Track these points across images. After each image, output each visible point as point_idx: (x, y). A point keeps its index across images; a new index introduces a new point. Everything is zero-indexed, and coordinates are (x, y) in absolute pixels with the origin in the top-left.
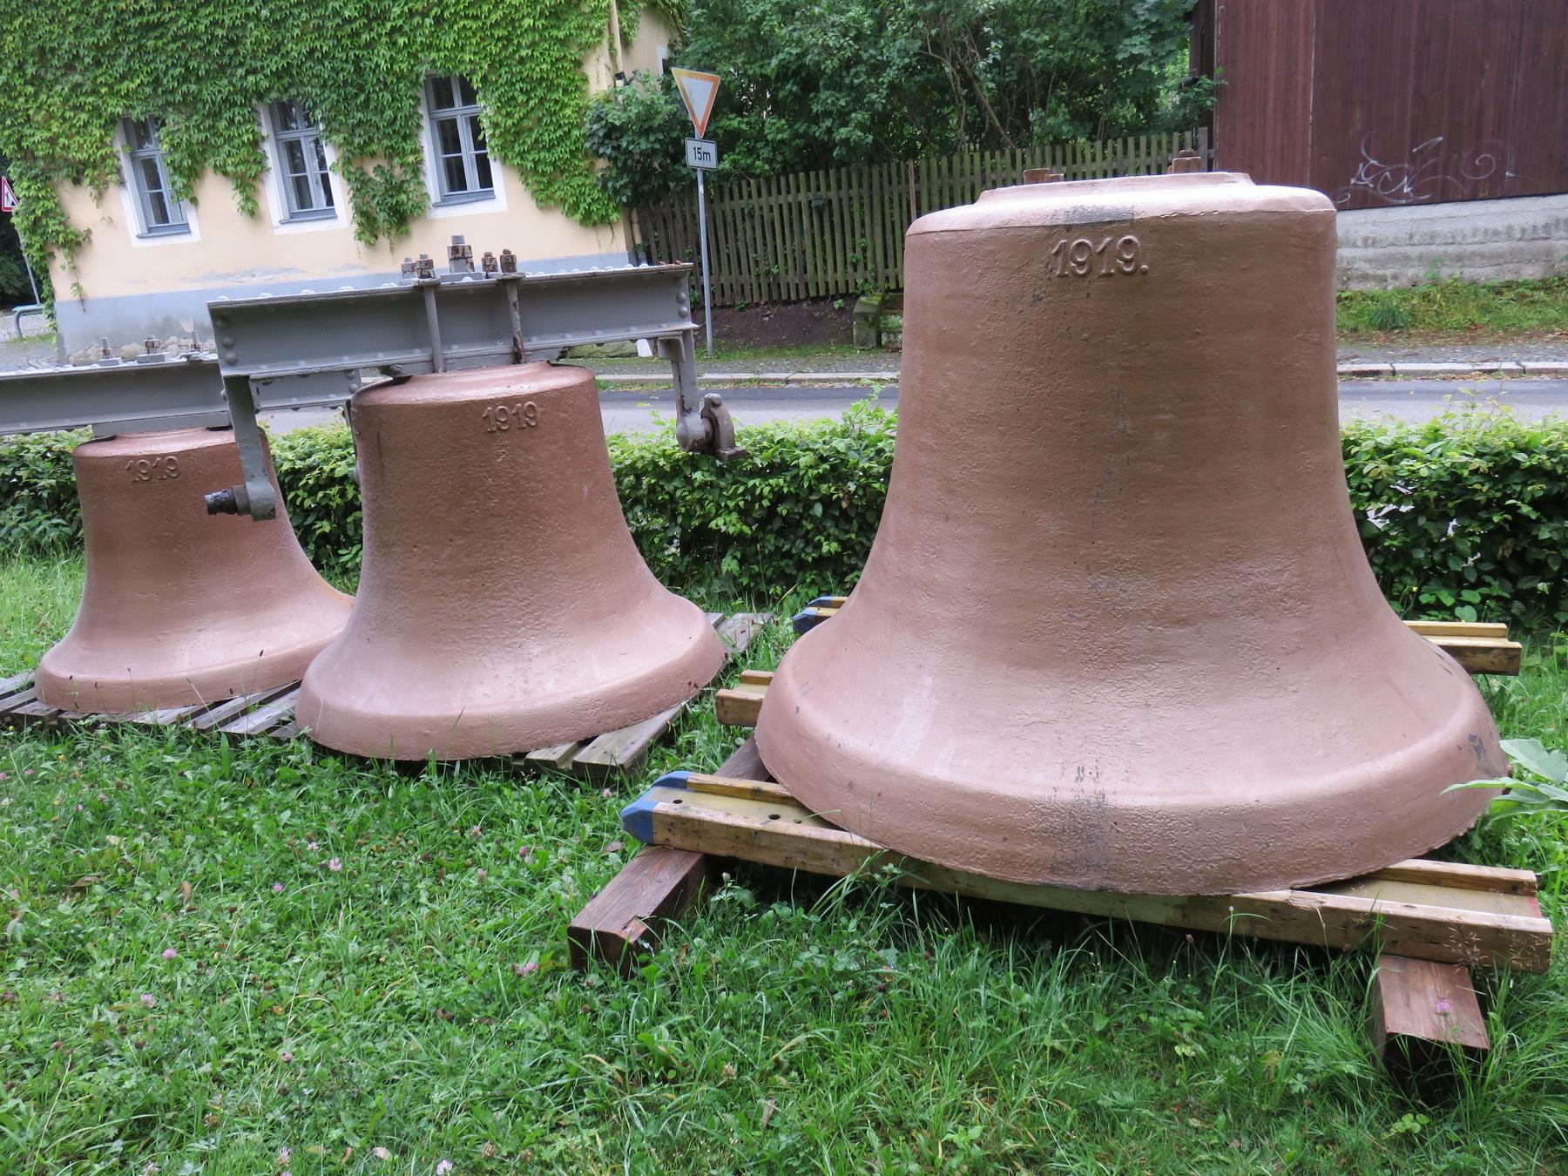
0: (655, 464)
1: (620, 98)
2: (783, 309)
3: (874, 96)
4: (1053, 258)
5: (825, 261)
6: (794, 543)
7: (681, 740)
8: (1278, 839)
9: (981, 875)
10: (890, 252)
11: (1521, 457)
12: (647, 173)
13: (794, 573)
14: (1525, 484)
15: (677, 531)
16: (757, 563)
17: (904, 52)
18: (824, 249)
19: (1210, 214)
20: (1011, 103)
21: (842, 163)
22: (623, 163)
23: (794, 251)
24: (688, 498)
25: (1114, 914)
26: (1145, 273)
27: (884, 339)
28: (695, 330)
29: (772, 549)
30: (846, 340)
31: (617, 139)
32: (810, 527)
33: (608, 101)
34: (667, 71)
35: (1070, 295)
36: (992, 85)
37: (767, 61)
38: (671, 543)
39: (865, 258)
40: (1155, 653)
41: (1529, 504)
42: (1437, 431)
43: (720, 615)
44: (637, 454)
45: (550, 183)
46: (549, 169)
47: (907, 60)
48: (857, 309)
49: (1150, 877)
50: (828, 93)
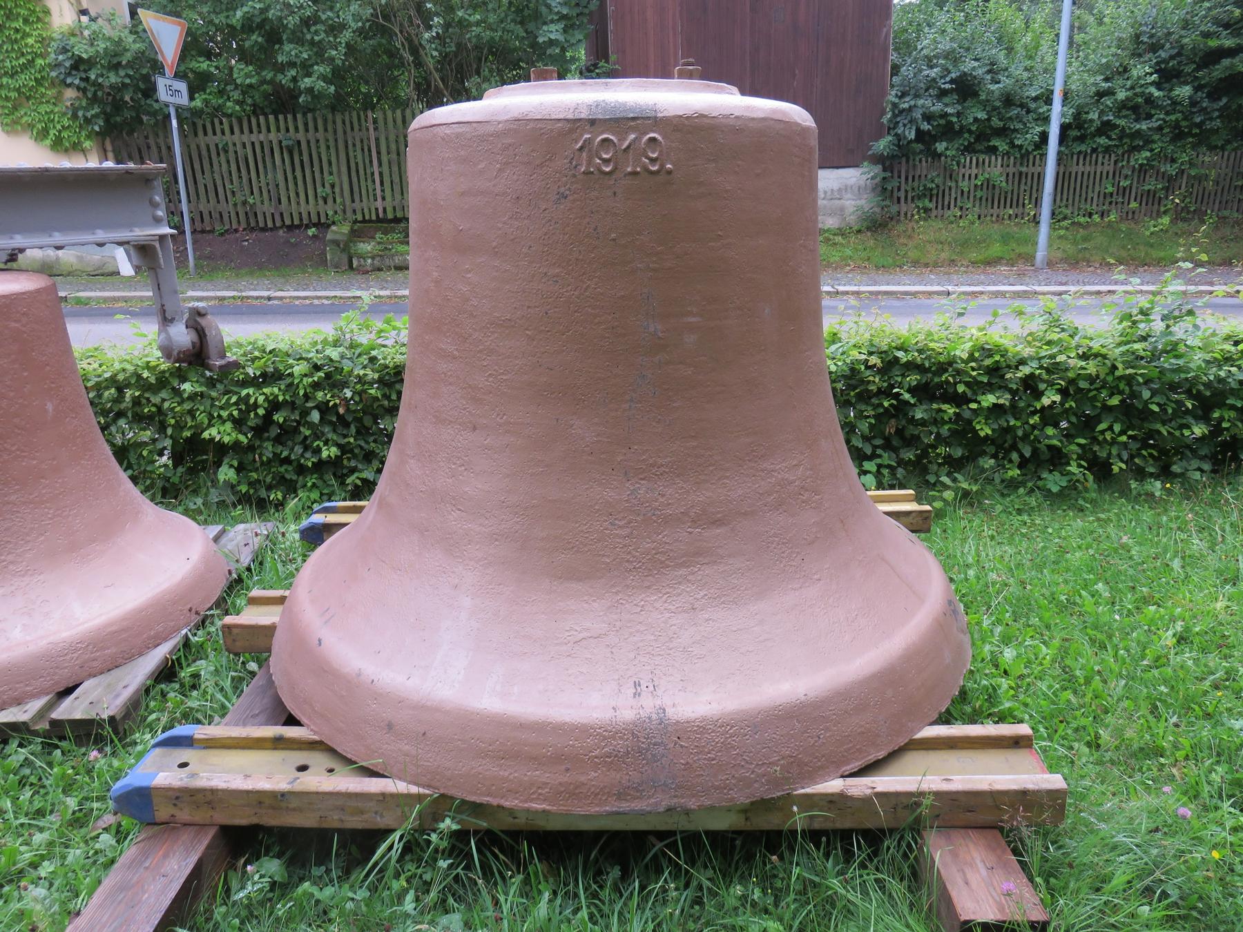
0: (139, 377)
1: (86, 33)
2: (262, 235)
3: (334, 53)
4: (577, 153)
5: (297, 194)
6: (292, 449)
7: (185, 674)
8: (827, 729)
9: (544, 811)
10: (356, 189)
11: (900, 354)
12: (118, 106)
13: (295, 478)
14: (903, 375)
15: (168, 443)
16: (256, 470)
17: (357, 18)
18: (296, 184)
19: (727, 117)
20: (452, 70)
21: (307, 110)
22: (92, 93)
23: (268, 184)
24: (178, 409)
25: (681, 828)
26: (669, 172)
27: (355, 263)
28: (172, 236)
29: (271, 456)
30: (321, 262)
31: (85, 71)
32: (308, 433)
33: (73, 35)
34: (133, 14)
35: (596, 193)
36: (435, 53)
37: (231, 13)
38: (161, 454)
39: (334, 193)
40: (696, 556)
41: (909, 391)
42: (835, 334)
43: (220, 527)
44: (117, 366)
45: (15, 108)
46: (13, 95)
47: (360, 24)
48: (329, 236)
49: (717, 788)
50: (292, 46)
